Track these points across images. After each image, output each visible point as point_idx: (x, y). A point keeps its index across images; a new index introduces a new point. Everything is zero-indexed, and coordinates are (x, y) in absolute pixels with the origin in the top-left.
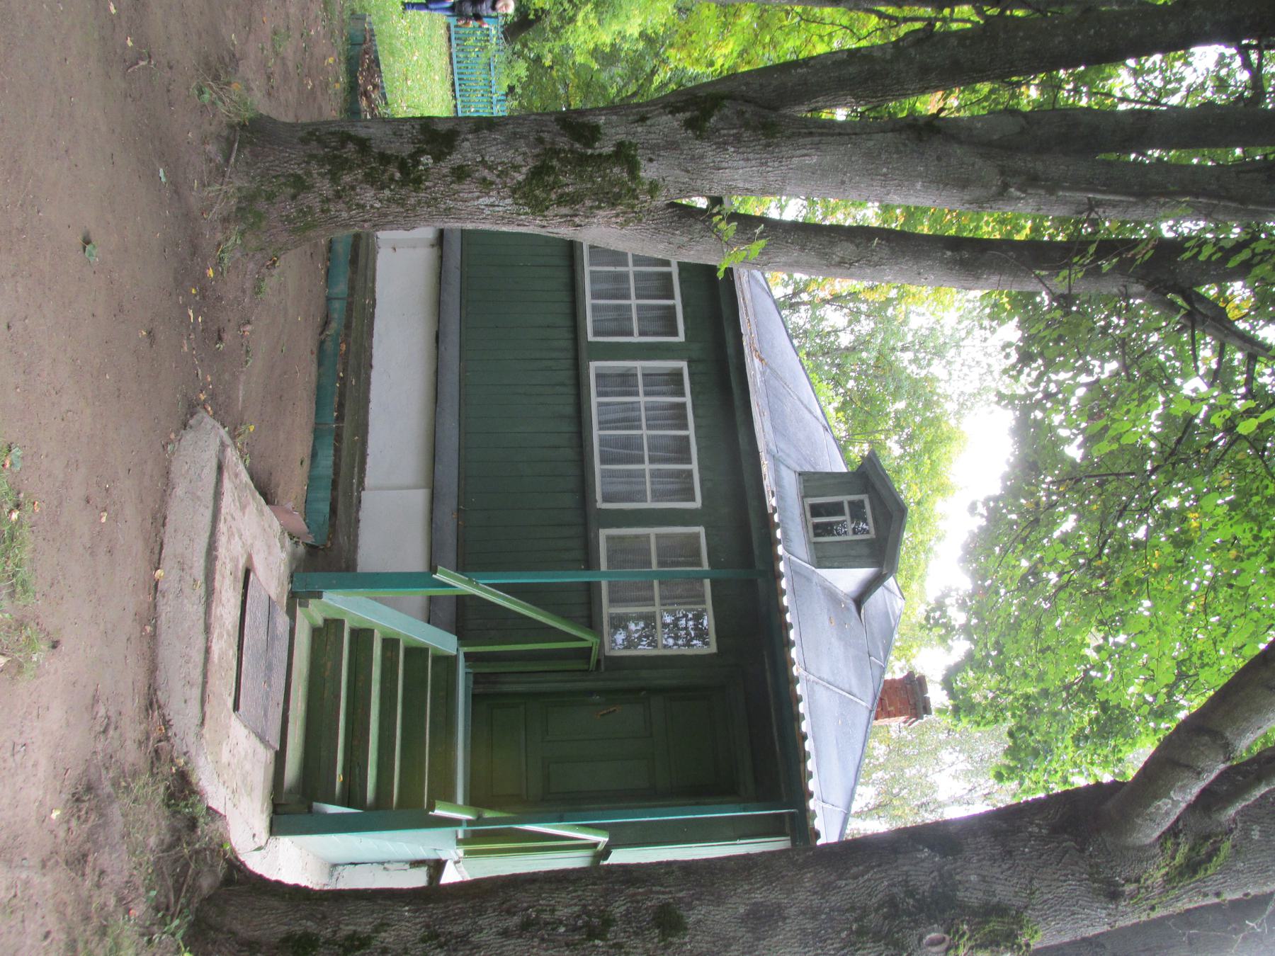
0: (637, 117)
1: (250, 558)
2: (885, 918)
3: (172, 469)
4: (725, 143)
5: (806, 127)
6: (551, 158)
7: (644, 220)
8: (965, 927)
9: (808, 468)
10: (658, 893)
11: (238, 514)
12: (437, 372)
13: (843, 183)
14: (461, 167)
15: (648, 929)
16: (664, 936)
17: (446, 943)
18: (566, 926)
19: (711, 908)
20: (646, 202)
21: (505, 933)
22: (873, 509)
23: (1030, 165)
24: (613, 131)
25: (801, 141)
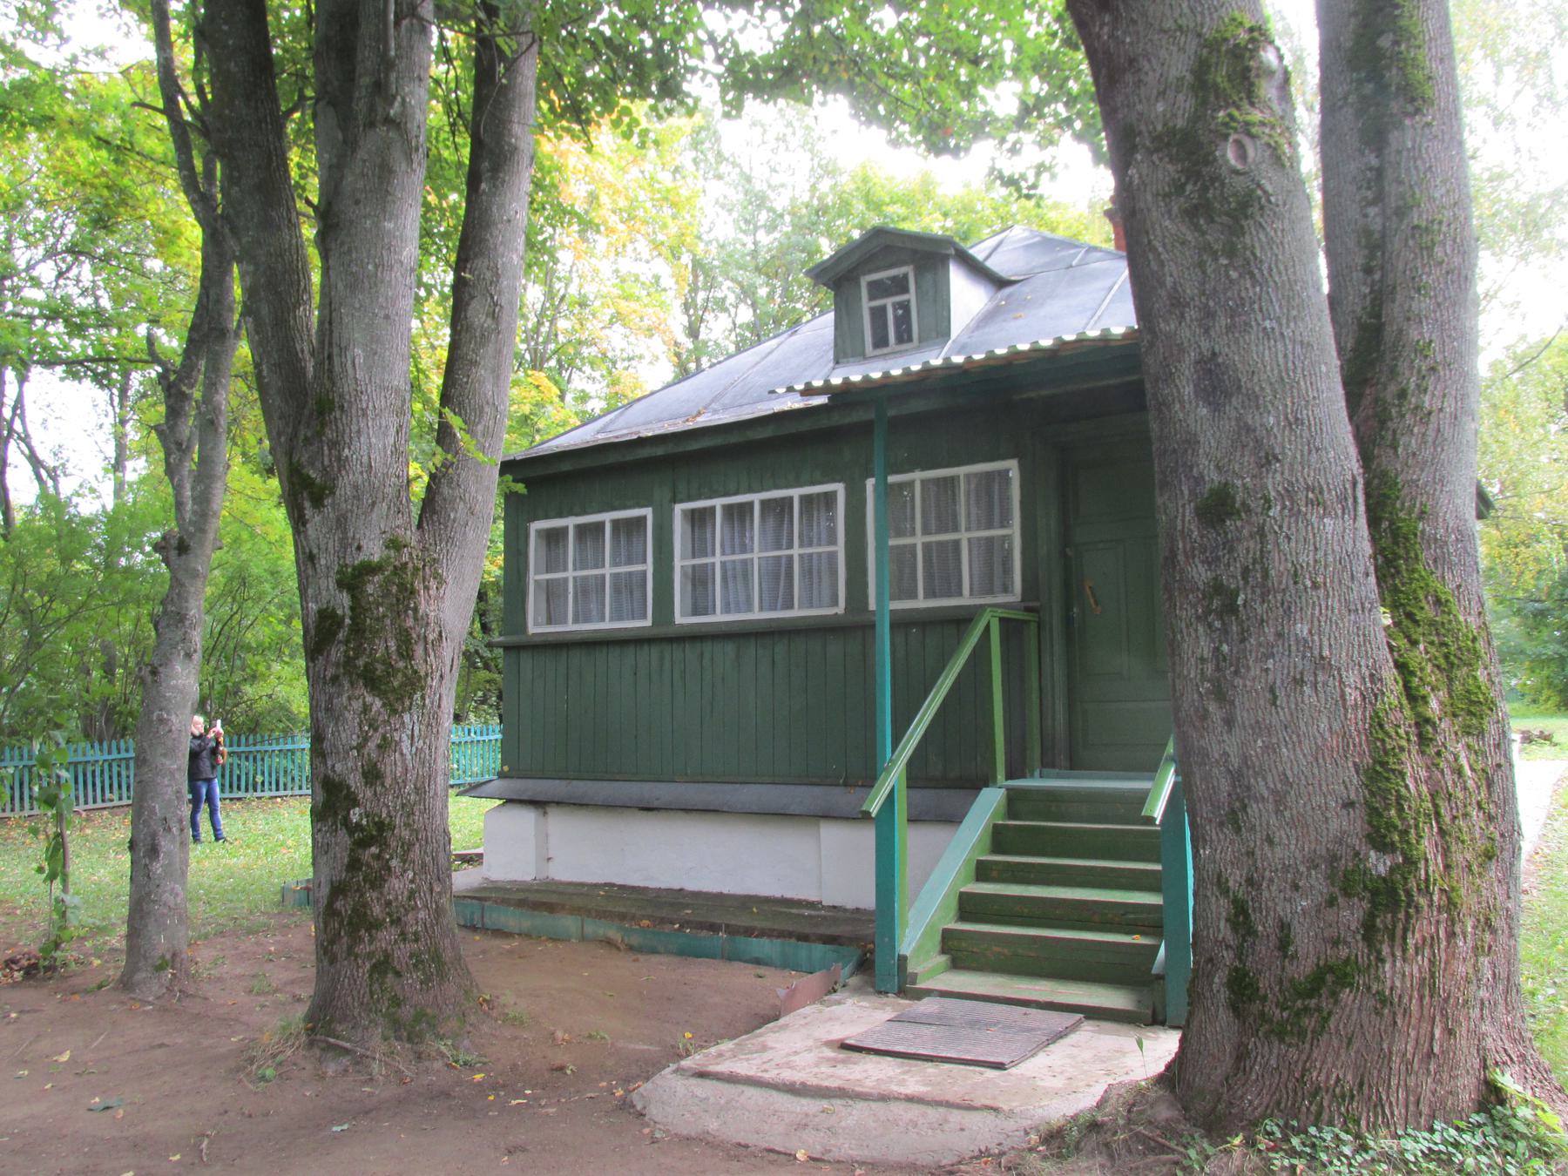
0: (309, 566)
1: (829, 1044)
2: (1213, 221)
3: (685, 1132)
4: (339, 459)
5: (322, 363)
6: (355, 667)
7: (436, 556)
8: (1221, 114)
9: (831, 355)
10: (1183, 521)
11: (767, 1055)
12: (687, 810)
13: (387, 317)
14: (365, 775)
15: (1226, 534)
16: (1232, 513)
17: (1242, 801)
18: (1221, 643)
19: (1201, 451)
20: (411, 554)
21: (1229, 722)
22: (877, 270)
23: (364, 93)
24: (324, 593)
25: (337, 369)
